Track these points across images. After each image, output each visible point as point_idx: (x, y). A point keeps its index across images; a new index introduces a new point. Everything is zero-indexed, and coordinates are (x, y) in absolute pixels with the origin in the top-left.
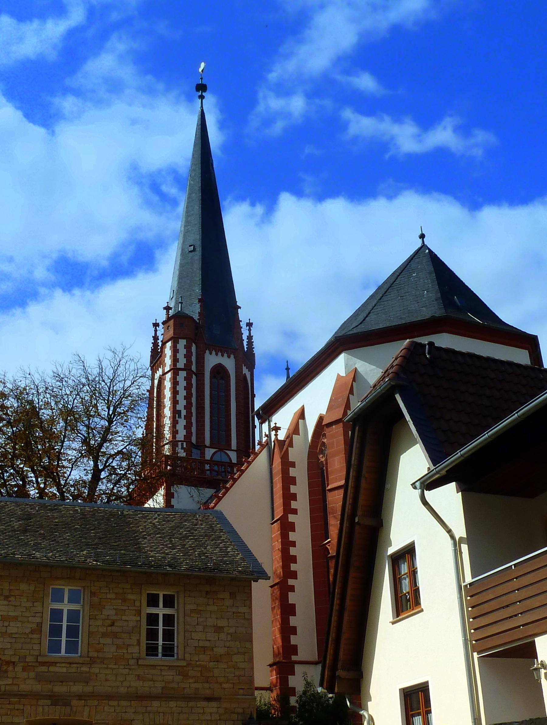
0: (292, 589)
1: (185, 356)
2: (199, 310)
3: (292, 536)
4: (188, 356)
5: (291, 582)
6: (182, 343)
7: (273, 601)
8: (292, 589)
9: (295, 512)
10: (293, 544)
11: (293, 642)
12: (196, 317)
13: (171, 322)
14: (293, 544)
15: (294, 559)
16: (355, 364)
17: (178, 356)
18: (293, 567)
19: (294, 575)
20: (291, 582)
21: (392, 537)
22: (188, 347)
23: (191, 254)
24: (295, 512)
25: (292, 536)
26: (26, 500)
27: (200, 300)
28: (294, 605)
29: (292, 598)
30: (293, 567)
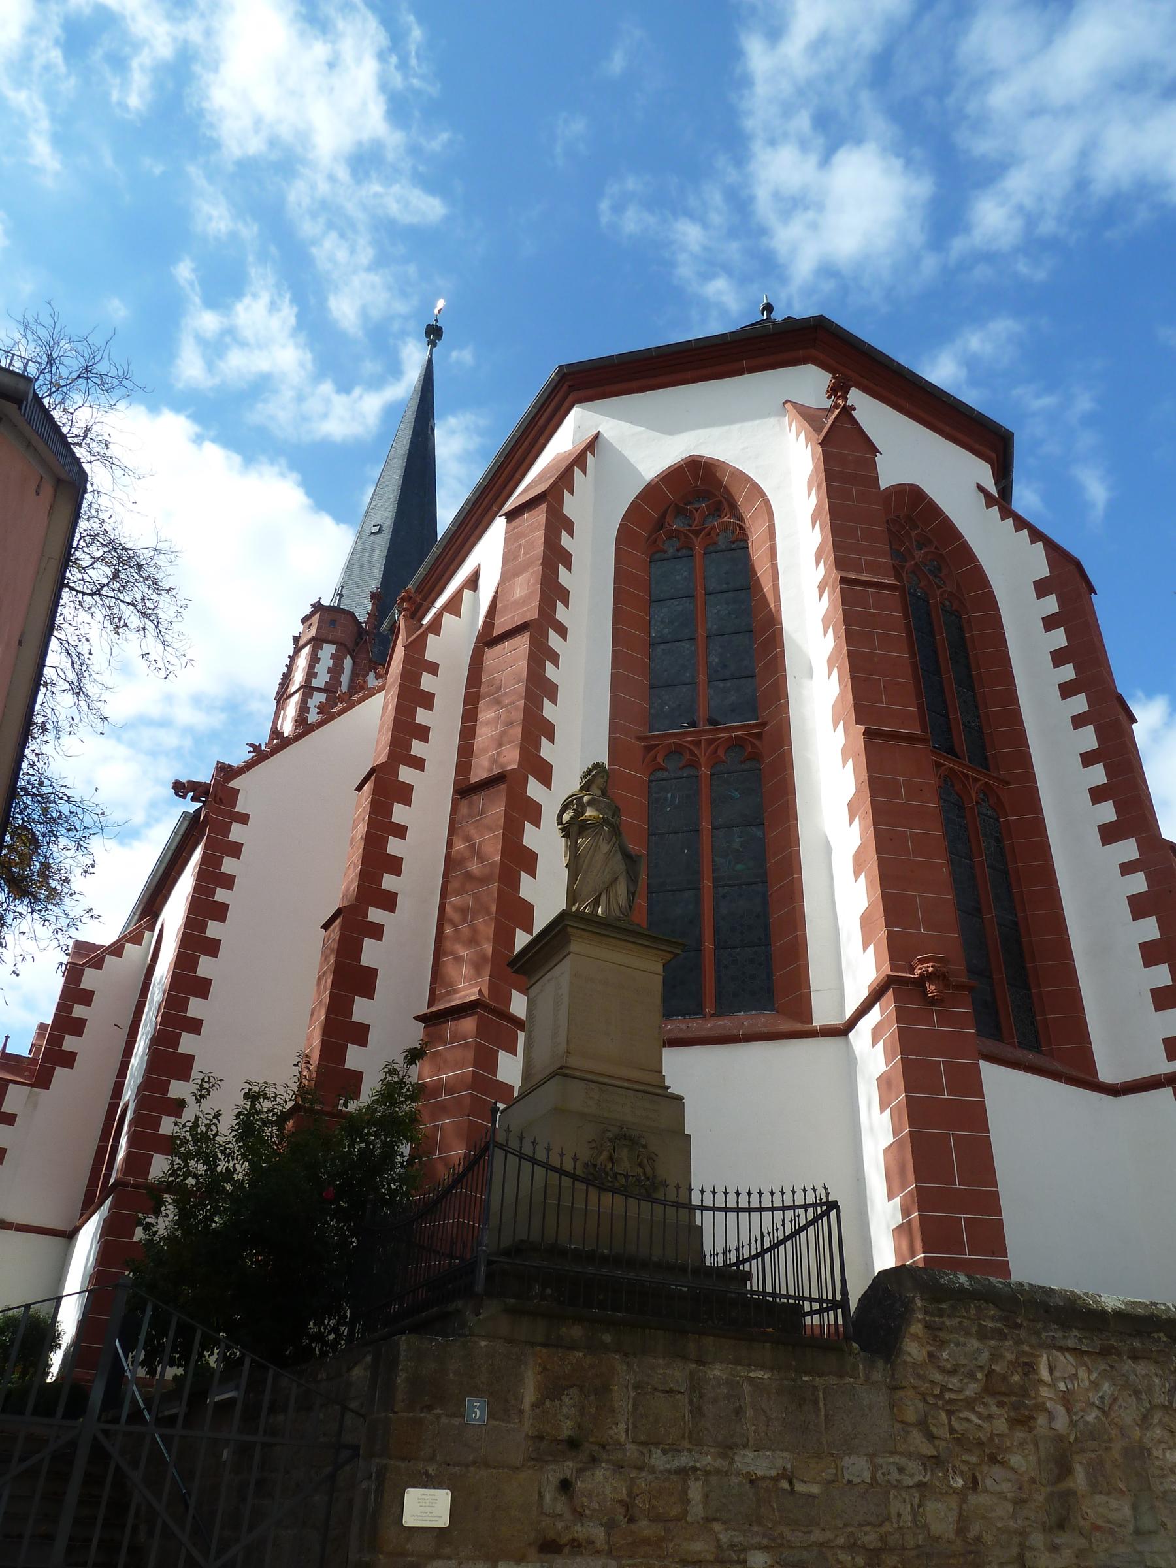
0: (376, 932)
1: (330, 670)
2: (369, 608)
3: (399, 813)
4: (336, 671)
5: (375, 915)
6: (328, 650)
7: (325, 958)
8: (376, 932)
9: (418, 764)
10: (401, 831)
11: (350, 1064)
12: (362, 616)
13: (315, 619)
14: (401, 831)
15: (395, 865)
16: (597, 426)
17: (317, 668)
18: (389, 882)
19: (389, 902)
20: (375, 915)
21: (866, 994)
22: (337, 659)
23: (373, 537)
24: (418, 764)
25: (399, 813)
26: (239, 1407)
27: (373, 596)
28: (372, 973)
29: (371, 953)
30: (389, 882)
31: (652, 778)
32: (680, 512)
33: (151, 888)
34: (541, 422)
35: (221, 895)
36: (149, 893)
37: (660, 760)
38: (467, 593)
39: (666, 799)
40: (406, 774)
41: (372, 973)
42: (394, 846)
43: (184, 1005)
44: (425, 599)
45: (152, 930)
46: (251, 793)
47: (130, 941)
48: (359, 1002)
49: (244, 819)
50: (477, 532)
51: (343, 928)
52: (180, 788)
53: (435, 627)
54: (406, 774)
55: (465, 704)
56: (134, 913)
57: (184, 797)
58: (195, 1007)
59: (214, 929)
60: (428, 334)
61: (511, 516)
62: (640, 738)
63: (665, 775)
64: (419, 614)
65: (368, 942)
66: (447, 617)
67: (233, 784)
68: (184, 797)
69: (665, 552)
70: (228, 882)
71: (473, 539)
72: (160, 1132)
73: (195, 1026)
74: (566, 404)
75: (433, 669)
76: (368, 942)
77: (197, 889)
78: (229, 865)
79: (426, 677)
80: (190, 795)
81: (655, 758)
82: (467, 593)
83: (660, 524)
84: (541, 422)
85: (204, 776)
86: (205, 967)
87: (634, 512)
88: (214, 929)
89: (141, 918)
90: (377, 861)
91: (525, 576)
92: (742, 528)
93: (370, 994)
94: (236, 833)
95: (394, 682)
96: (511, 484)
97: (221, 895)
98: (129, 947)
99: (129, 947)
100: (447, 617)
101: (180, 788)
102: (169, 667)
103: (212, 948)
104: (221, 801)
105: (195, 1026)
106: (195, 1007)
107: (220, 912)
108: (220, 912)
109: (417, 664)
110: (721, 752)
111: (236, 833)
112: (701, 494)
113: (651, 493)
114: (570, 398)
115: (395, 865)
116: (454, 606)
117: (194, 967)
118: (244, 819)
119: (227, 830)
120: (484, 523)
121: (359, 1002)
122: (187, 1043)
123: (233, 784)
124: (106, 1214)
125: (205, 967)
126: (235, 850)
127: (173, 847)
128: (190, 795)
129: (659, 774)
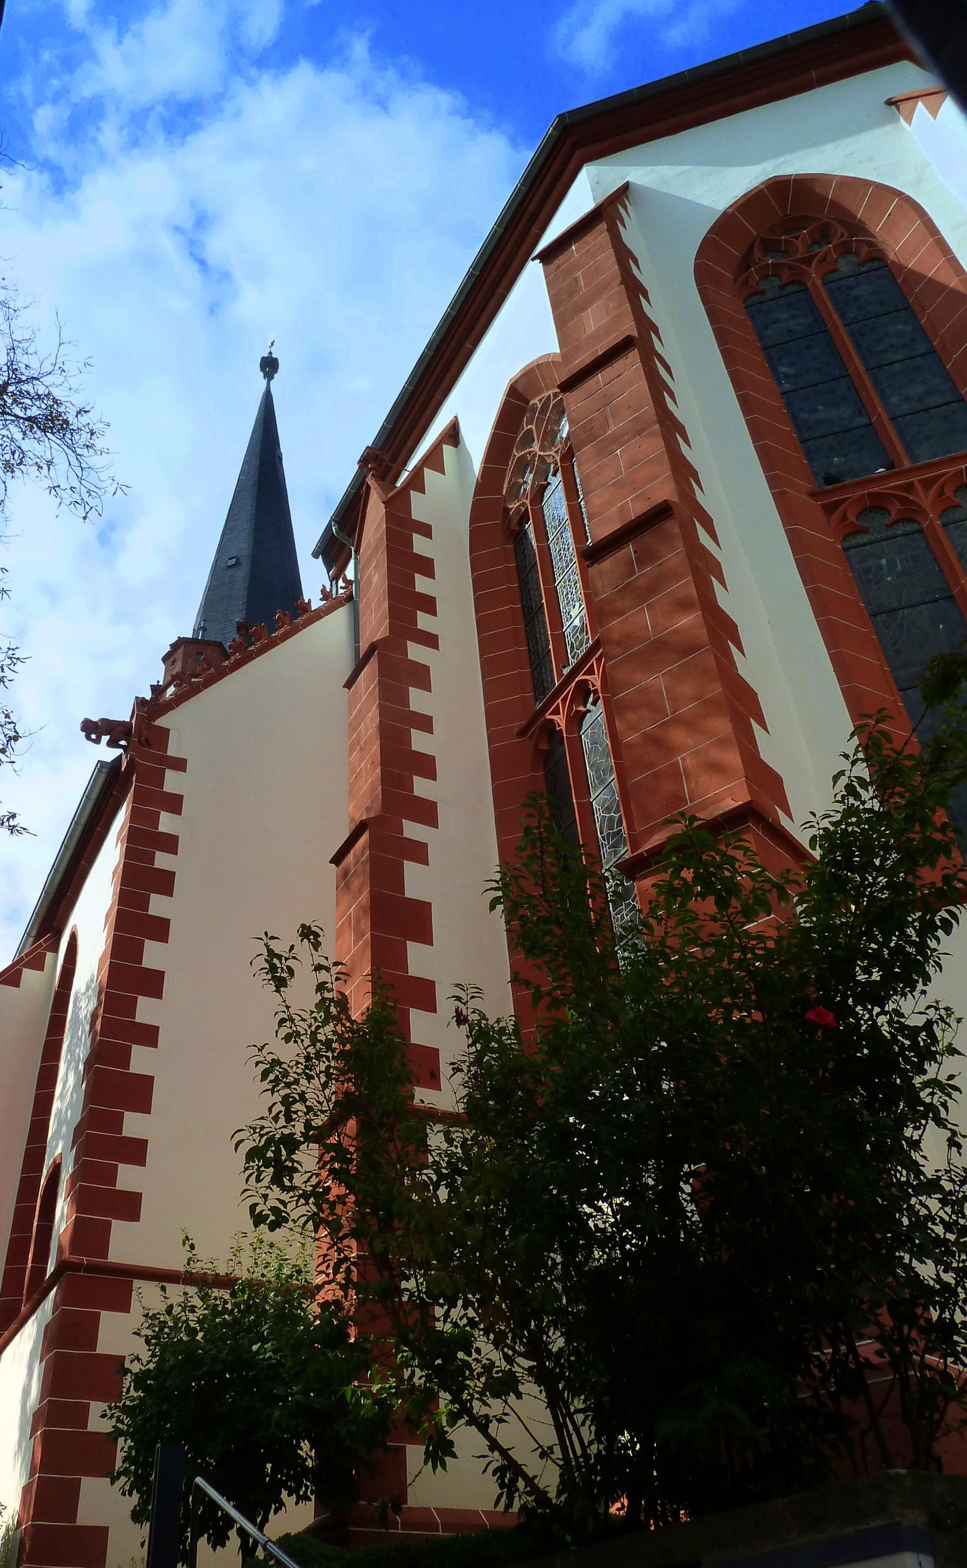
0: (419, 852)
5: (412, 830)
8: (419, 852)
15: (426, 766)
18: (421, 787)
19: (427, 813)
20: (412, 830)
23: (230, 572)
29: (417, 882)
30: (421, 787)
31: (847, 544)
32: (769, 246)
33: (52, 891)
34: (531, 208)
35: (162, 860)
36: (39, 920)
37: (851, 517)
38: (447, 450)
39: (880, 567)
40: (416, 652)
41: (423, 909)
42: (419, 741)
43: (131, 1008)
44: (394, 459)
45: (55, 949)
46: (183, 728)
47: (28, 966)
48: (414, 949)
49: (180, 765)
50: (505, 282)
51: (372, 844)
52: (92, 729)
53: (417, 481)
54: (416, 652)
55: (19, 1200)
56: (28, 934)
57: (97, 741)
58: (146, 1010)
59: (158, 905)
60: (263, 367)
61: (546, 257)
62: (813, 495)
63: (865, 538)
64: (392, 473)
65: (409, 867)
66: (428, 473)
67: (161, 722)
68: (97, 741)
69: (763, 292)
70: (170, 844)
71: (438, 396)
72: (119, 1187)
73: (149, 1035)
74: (571, 166)
75: (426, 530)
76: (409, 867)
77: (130, 854)
78: (166, 823)
79: (418, 540)
80: (105, 739)
81: (844, 517)
82: (447, 450)
83: (746, 262)
84: (531, 208)
85: (123, 713)
86: (153, 955)
87: (708, 249)
88: (158, 905)
89: (37, 938)
90: (400, 765)
91: (598, 304)
92: (871, 244)
93: (426, 937)
94: (172, 782)
95: (375, 552)
96: (431, 407)
97: (162, 860)
98: (27, 973)
99: (27, 973)
100: (428, 473)
101: (92, 729)
102: (89, 500)
103: (160, 929)
104: (148, 743)
105: (149, 1035)
106: (146, 1010)
107: (165, 883)
108: (165, 883)
109: (402, 527)
110: (948, 492)
111: (172, 782)
112: (793, 224)
113: (727, 225)
114: (577, 156)
115: (426, 766)
116: (434, 459)
117: (138, 955)
118: (180, 765)
119: (159, 780)
120: (511, 272)
121: (414, 949)
122: (141, 1060)
123: (161, 722)
124: (49, 1316)
125: (153, 955)
126: (175, 804)
127: (95, 795)
128: (105, 739)
129: (854, 541)
